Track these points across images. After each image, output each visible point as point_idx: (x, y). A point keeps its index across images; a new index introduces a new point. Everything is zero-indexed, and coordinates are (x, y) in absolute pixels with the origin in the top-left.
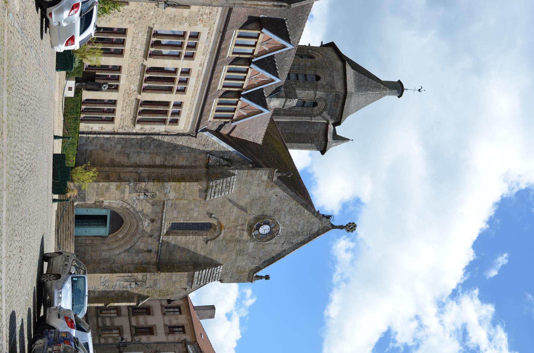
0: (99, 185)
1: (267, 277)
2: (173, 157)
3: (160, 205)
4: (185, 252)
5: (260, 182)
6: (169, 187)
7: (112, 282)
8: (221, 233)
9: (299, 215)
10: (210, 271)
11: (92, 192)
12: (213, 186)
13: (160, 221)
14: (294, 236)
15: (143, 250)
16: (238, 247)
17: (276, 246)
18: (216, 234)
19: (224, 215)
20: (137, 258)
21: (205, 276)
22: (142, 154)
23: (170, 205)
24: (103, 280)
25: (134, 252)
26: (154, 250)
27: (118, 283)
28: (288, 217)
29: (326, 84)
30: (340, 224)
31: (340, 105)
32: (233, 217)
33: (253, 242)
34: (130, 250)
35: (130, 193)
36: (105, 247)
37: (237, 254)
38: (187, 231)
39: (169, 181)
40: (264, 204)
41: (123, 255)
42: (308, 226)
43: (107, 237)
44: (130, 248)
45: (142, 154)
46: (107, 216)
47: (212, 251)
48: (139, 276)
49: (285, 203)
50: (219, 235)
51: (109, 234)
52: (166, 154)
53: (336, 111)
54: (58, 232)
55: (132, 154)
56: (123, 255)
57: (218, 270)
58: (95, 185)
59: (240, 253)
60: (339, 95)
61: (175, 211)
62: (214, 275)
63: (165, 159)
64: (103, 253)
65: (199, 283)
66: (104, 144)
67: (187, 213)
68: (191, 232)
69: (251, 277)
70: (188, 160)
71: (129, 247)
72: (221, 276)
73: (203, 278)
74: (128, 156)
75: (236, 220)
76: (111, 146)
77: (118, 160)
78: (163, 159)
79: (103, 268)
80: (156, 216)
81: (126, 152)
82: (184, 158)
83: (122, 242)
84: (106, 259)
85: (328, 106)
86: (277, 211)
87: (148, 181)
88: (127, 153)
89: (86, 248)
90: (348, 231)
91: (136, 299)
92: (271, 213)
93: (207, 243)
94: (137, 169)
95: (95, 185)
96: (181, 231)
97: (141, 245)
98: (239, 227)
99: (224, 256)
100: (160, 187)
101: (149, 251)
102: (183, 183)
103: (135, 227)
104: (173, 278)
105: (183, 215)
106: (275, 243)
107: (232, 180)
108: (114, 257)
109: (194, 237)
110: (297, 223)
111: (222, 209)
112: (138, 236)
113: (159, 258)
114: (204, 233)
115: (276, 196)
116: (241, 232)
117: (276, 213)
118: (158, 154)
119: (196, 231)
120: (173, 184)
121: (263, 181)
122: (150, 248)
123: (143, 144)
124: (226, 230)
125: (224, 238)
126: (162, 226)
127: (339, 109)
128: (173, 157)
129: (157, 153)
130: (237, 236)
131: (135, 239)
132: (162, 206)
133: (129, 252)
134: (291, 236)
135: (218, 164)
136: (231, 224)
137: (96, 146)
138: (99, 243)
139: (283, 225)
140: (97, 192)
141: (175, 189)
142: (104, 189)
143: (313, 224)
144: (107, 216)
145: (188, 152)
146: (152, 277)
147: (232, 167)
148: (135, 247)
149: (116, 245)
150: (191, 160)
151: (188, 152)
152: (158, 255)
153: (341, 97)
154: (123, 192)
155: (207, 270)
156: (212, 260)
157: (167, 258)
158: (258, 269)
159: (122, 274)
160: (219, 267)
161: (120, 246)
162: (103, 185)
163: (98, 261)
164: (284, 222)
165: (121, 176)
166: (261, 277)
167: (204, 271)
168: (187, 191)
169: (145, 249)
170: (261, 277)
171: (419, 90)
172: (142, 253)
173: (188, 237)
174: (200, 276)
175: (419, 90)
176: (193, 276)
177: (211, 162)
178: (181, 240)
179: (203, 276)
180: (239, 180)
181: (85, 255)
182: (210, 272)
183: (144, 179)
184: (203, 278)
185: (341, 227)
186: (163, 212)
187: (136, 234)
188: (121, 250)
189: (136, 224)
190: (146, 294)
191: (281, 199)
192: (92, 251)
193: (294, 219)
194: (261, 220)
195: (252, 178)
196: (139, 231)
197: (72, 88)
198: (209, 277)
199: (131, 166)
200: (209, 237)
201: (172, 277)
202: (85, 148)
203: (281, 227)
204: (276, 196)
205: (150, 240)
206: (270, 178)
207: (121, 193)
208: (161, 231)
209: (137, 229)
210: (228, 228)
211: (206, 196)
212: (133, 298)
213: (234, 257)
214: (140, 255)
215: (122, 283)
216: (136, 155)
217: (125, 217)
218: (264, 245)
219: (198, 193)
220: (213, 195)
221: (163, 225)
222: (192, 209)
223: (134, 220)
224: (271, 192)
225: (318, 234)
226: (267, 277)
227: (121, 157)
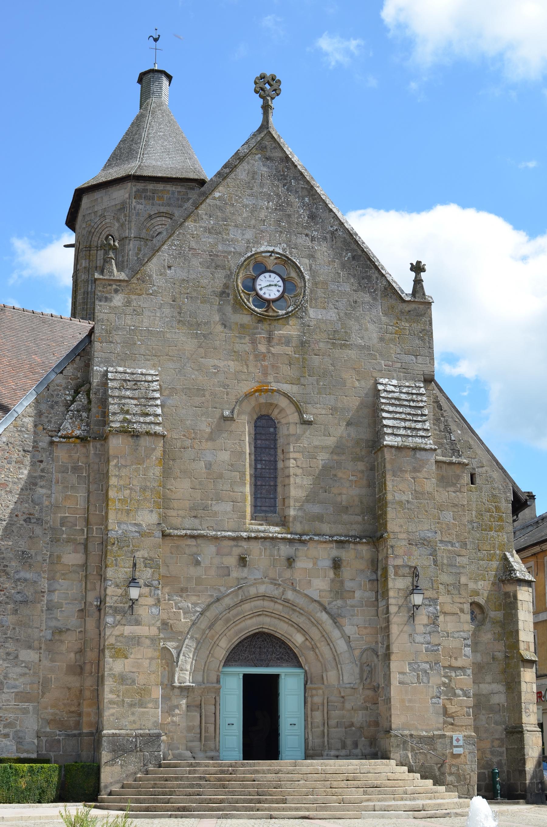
0: (111, 702)
1: (418, 268)
2: (62, 524)
3: (197, 546)
4: (340, 475)
5: (129, 310)
6: (124, 527)
7: (417, 653)
8: (278, 391)
9: (229, 209)
10: (386, 408)
11: (131, 718)
12: (125, 420)
13: (244, 544)
15: (333, 581)
16: (322, 345)
17: (318, 255)
18: (283, 403)
19: (225, 386)
20: (358, 594)
21: (405, 420)
22: (55, 597)
23: (197, 521)
24: (411, 677)
25: (339, 602)
26: (335, 553)
27: (419, 639)
28: (234, 233)
29: (118, 220)
30: (261, 111)
31: (160, 186)
32: (233, 366)
33: (306, 311)
34: (334, 611)
35: (138, 623)
36: (331, 676)
37: (342, 346)
38: (280, 473)
40: (194, 294)
41: (349, 629)
42: (262, 185)
43: (306, 672)
44: (327, 613)
45: (55, 597)
46: (246, 677)
47: (334, 409)
48: (397, 584)
49: (193, 244)
50: (286, 395)
51: (300, 666)
52: (55, 540)
53: (173, 193)
54: (184, 809)
55: (53, 623)
56: (349, 629)
57: (390, 388)
58: (112, 711)
59: (339, 339)
60: (138, 191)
61: (215, 508)
62: (403, 396)
63: (68, 541)
64: (346, 679)
65: (421, 433)
66: (17, 694)
67: (221, 476)
68: (280, 465)
69: (413, 306)
71: (324, 616)
72: (414, 379)
73: (408, 424)
74: (61, 632)
75: (236, 355)
76: (24, 675)
77: (72, 655)
78: (70, 547)
80: (229, 554)
81: (49, 637)
82: (66, 498)
83: (315, 633)
84: (362, 671)
85: (163, 209)
86: (214, 262)
88: (53, 633)
89: (333, 722)
90: (277, 91)
91: (509, 588)
92: (220, 275)
93: (309, 423)
95: (112, 711)
96: (279, 489)
97: (320, 586)
98: (262, 348)
99: (350, 377)
100: (120, 548)
101: (337, 564)
102: (112, 494)
103: (266, 603)
104: (404, 498)
105: (227, 487)
106: (311, 257)
107: (119, 376)
108: (357, 653)
109: (292, 455)
110: (252, 212)
111: (207, 393)
112: (290, 595)
113: (356, 539)
114: (283, 431)
115: (169, 267)
116: (275, 341)
117: (219, 263)
118: (55, 560)
119: (279, 451)
121: (128, 303)
122: (328, 563)
123: (19, 597)
124: (270, 379)
125: (296, 381)
126: (256, 538)
127: (169, 187)
128: (62, 524)
129: (52, 563)
130: (289, 350)
131: (301, 601)
132: (199, 541)
133: (340, 615)
134: (289, 223)
135: (84, 415)
136: (251, 369)
137: (25, 711)
139: (257, 242)
140: (132, 705)
141: (128, 512)
142: (123, 688)
143: (253, 175)
144: (246, 677)
145: (50, 488)
146: (399, 551)
148: (325, 601)
149: (324, 649)
150: (73, 479)
151: (50, 488)
152: (348, 542)
153: (140, 186)
154: (136, 640)
155: (385, 415)
156: (362, 405)
157: (360, 518)
158: (390, 290)
159: (394, 630)
160: (380, 387)
161: (329, 641)
162: (111, 692)
163: (370, 693)
164: (248, 242)
166: (418, 282)
167: (385, 422)
168: (135, 482)
169: (331, 574)
170: (418, 282)
171: (156, 40)
172: (342, 582)
173: (292, 471)
174: (402, 432)
175: (156, 40)
176: (398, 448)
177: (77, 432)
178: (301, 487)
179: (403, 424)
180: (123, 359)
181: (352, 725)
182: (391, 409)
184: (408, 424)
185: (266, 108)
186: (216, 538)
187: (286, 601)
188: (336, 634)
189: (259, 603)
190: (495, 564)
192: (343, 708)
193: (240, 220)
195: (118, 329)
196: (276, 593)
198: (408, 410)
200: (294, 417)
201: (400, 503)
202: (30, 738)
203: (262, 249)
204: (169, 267)
205: (301, 564)
206: (119, 285)
207: (139, 644)
208: (272, 538)
209: (272, 599)
210: (265, 374)
211: (148, 433)
212: (507, 595)
213: (352, 353)
214: (348, 585)
215: (420, 629)
217: (241, 631)
218: (316, 284)
220: (151, 419)
221: (253, 535)
222: (209, 466)
223: (246, 606)
224: (159, 281)
226: (418, 268)
227: (63, 648)
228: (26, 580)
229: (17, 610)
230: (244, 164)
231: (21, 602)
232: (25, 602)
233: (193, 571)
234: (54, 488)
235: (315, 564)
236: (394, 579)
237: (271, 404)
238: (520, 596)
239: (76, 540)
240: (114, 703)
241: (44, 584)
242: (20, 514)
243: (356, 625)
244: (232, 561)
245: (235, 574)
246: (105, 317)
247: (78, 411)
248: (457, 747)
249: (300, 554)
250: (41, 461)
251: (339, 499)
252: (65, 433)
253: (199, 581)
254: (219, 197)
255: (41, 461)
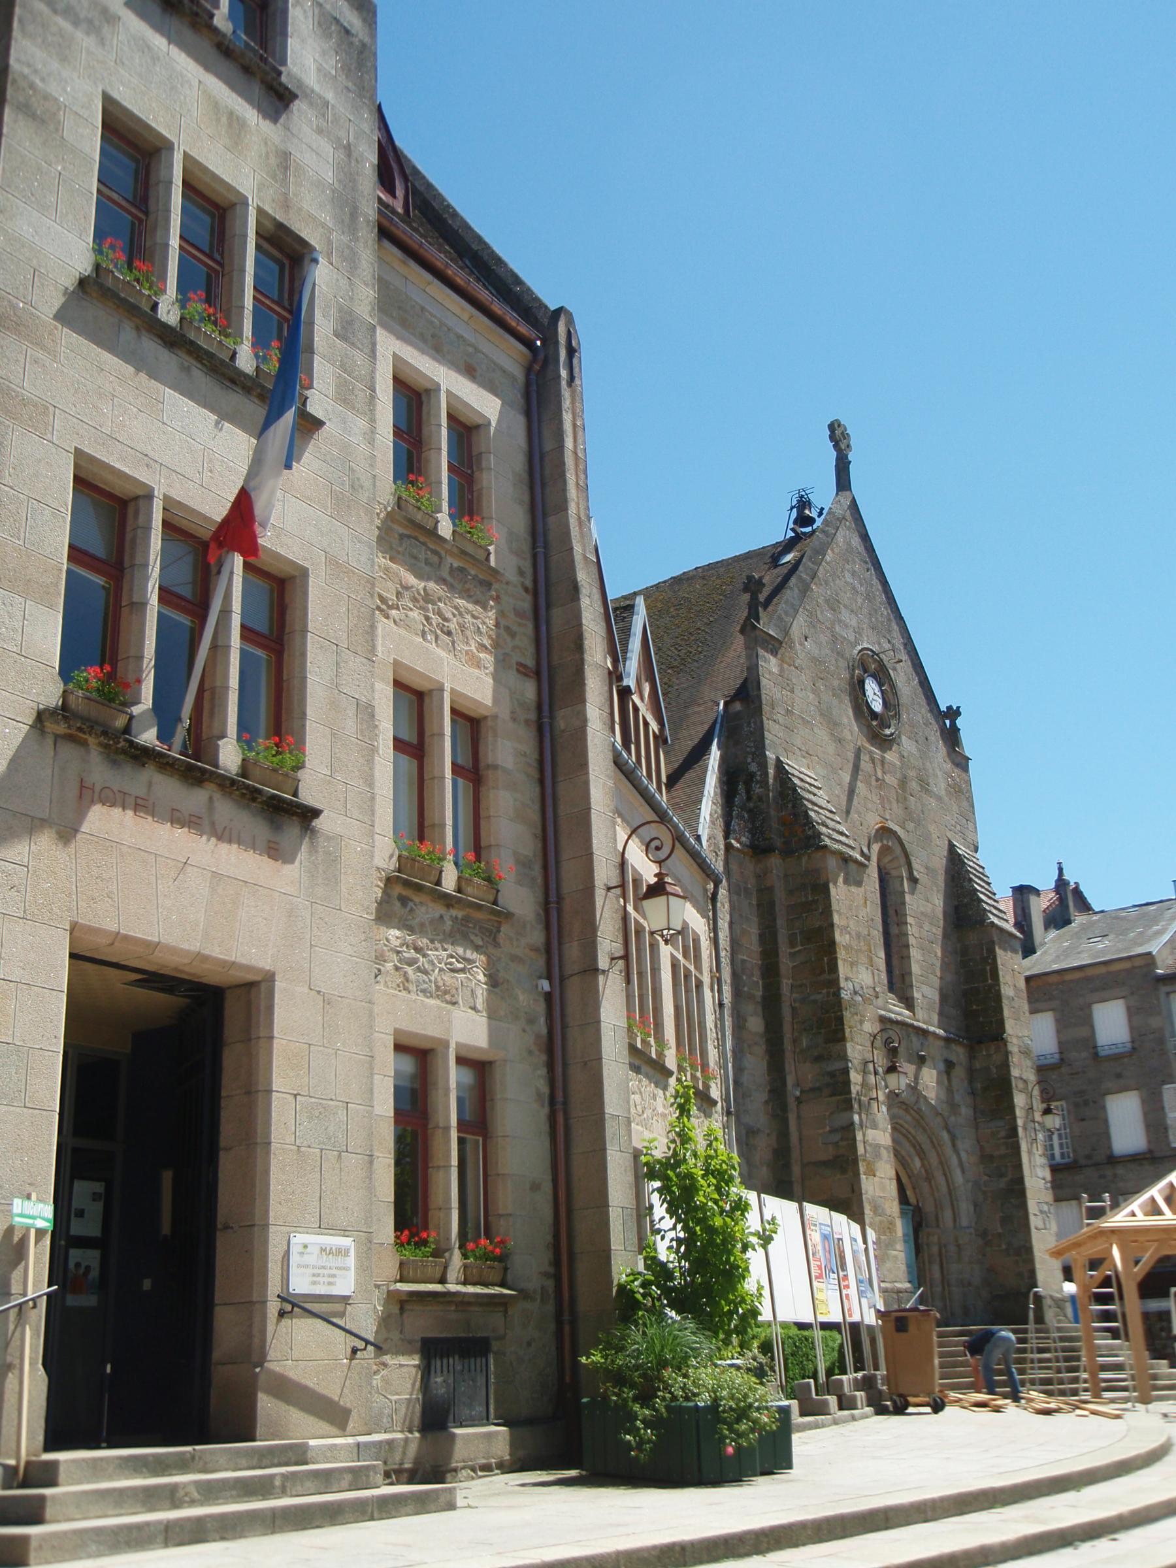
39: (833, 984)
64: (964, 1222)
71: (945, 1136)
74: (753, 1132)
79: (1005, 1220)
83: (933, 1160)
87: (844, 1058)
92: (843, 664)
94: (792, 1104)
115: (806, 638)
120: (843, 970)
138: (935, 1239)
147: (753, 767)
161: (943, 1164)
165: (823, 1157)
181: (970, 1284)
183: (832, 1075)
191: (812, 625)
197: (76, 1216)
199: (785, 1122)
219: (853, 889)
225: (865, 538)
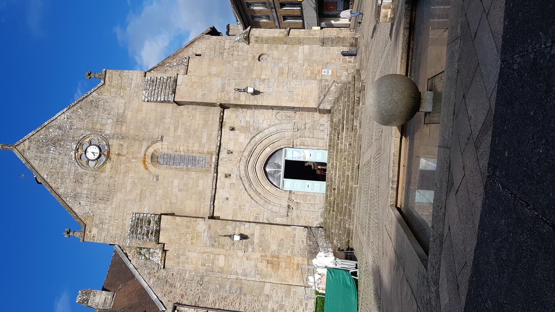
14: (58, 140)
15: (241, 132)
20: (248, 119)
35: (253, 235)
44: (256, 135)
46: (285, 177)
55: (253, 273)
66: (286, 297)
69: (107, 79)
70: (187, 259)
75: (126, 172)
97: (243, 138)
121: (97, 226)
128: (205, 265)
131: (249, 148)
144: (285, 177)
188: (267, 132)
194: (105, 154)
216: (248, 271)
222: (180, 190)
228: (230, 288)
229: (245, 294)
230: (30, 161)
231: (241, 291)
232: (241, 289)
233: (231, 202)
234: (187, 268)
235: (232, 140)
236: (241, 101)
237: (152, 156)
238: (257, 35)
239: (212, 259)
240: (292, 251)
241: (233, 277)
242: (197, 288)
243: (264, 119)
244: (227, 181)
245: (234, 181)
246: (103, 238)
247: (150, 253)
248: (328, 73)
249: (226, 147)
250: (173, 274)
251: (200, 125)
252: (160, 261)
253: (236, 199)
254: (47, 175)
255: (173, 274)
